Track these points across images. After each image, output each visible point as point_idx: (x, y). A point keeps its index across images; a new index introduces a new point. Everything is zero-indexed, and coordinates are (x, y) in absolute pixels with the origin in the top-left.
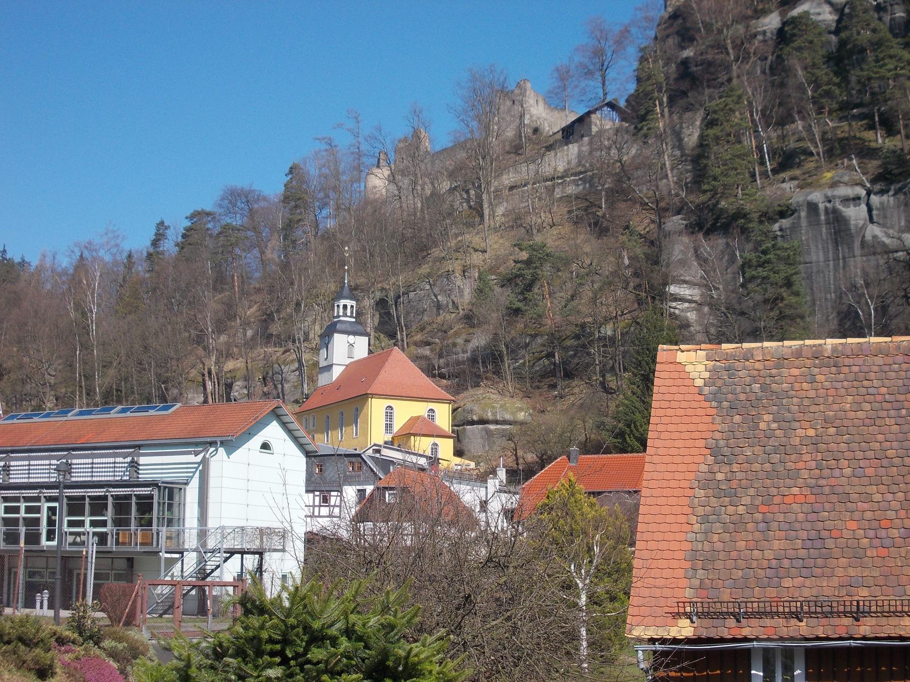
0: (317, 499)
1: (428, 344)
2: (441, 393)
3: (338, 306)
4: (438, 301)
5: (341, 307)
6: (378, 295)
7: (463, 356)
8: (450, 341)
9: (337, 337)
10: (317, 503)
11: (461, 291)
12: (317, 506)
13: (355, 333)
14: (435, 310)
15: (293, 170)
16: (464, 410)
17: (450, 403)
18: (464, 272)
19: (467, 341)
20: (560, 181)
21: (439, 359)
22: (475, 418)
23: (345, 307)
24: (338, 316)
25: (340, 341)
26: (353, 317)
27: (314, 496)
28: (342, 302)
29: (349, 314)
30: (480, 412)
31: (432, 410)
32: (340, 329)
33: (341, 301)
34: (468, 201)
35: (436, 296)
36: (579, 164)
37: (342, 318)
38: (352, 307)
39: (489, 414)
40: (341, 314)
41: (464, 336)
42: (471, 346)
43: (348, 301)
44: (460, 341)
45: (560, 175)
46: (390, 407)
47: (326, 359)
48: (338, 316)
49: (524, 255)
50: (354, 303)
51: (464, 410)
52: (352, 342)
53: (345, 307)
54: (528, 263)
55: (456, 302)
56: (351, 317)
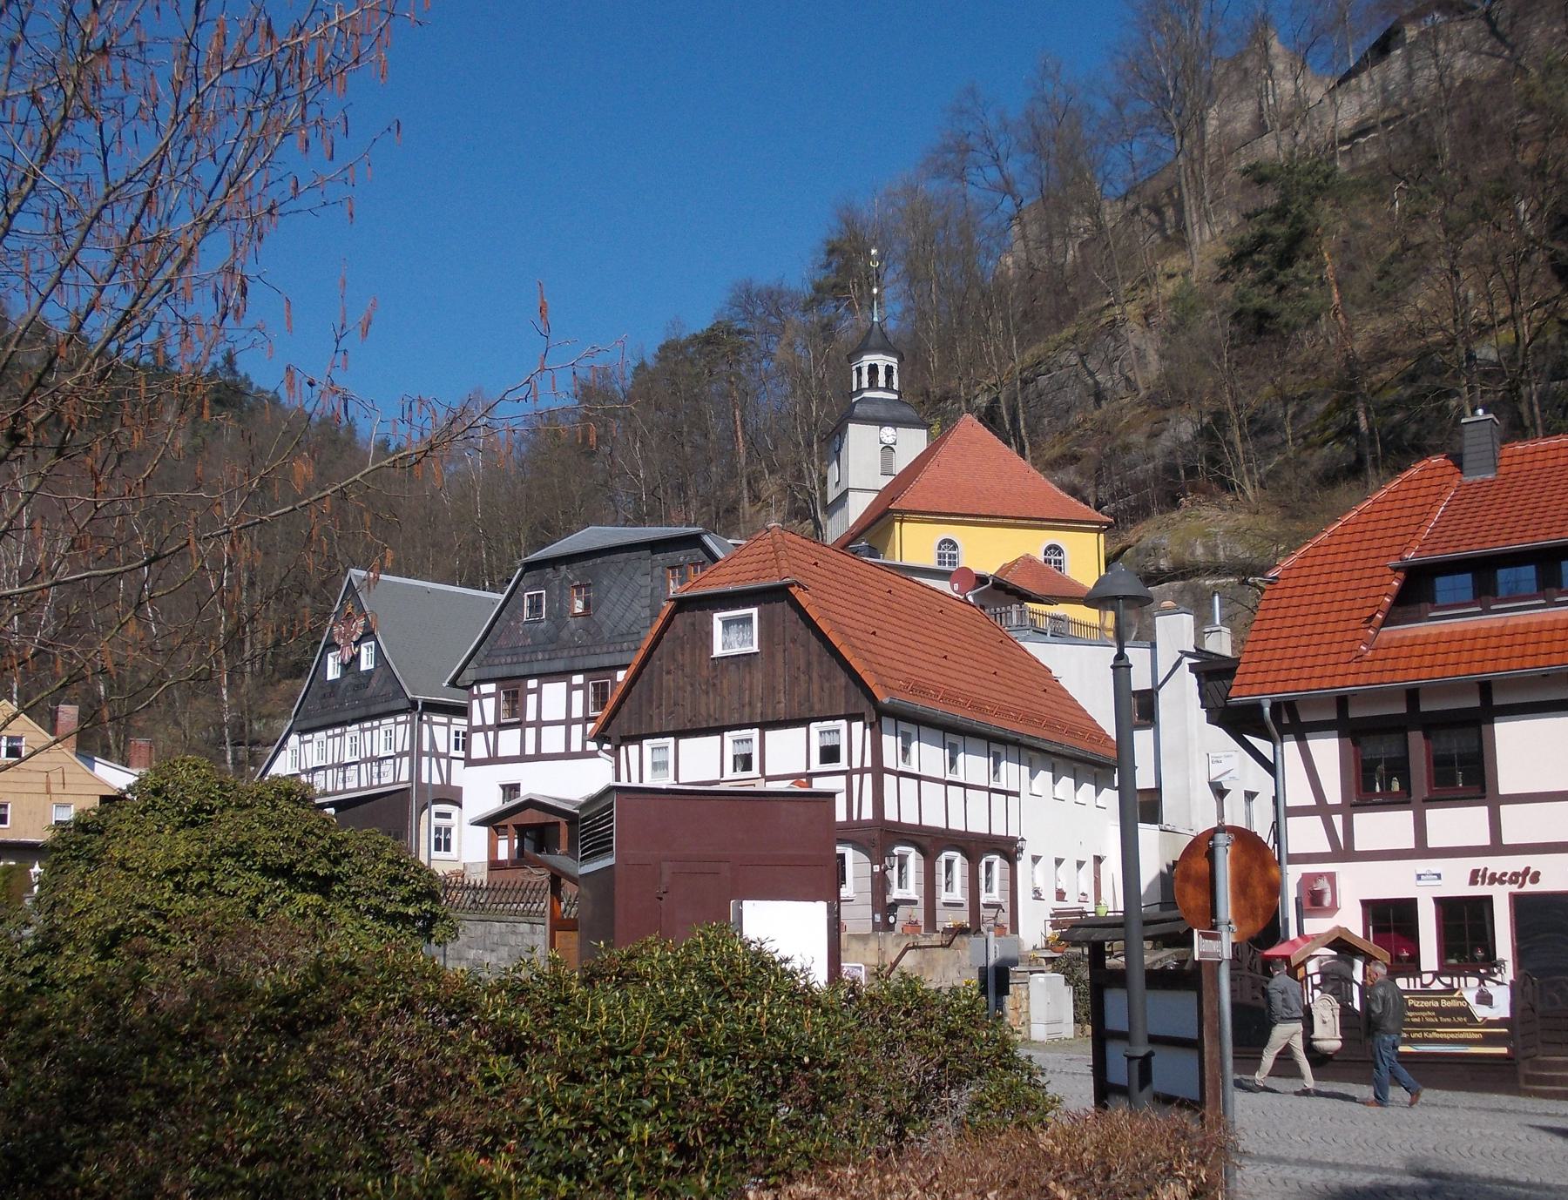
0: (578, 696)
1: (1075, 459)
2: (1077, 508)
3: (859, 370)
4: (1097, 383)
5: (865, 371)
6: (983, 401)
7: (1144, 470)
8: (1119, 442)
9: (854, 430)
10: (577, 712)
11: (1140, 354)
12: (577, 721)
13: (896, 423)
14: (1092, 400)
15: (1210, 783)
16: (1138, 552)
17: (1099, 531)
18: (1146, 317)
19: (1154, 435)
20: (1346, 148)
21: (1097, 486)
22: (1164, 564)
23: (873, 369)
24: (860, 390)
25: (862, 442)
26: (892, 391)
27: (571, 688)
28: (868, 360)
29: (882, 382)
30: (1176, 549)
31: (1054, 549)
32: (862, 415)
33: (865, 358)
34: (1161, 229)
35: (1091, 374)
36: (1385, 105)
37: (867, 394)
38: (889, 370)
39: (1200, 551)
40: (865, 384)
41: (1146, 428)
42: (1165, 441)
43: (881, 356)
44: (1137, 438)
45: (1346, 135)
46: (951, 542)
47: (837, 484)
48: (860, 390)
49: (1270, 198)
50: (893, 361)
51: (1138, 552)
52: (889, 440)
53: (873, 369)
54: (1280, 213)
55: (1133, 379)
56: (888, 388)
